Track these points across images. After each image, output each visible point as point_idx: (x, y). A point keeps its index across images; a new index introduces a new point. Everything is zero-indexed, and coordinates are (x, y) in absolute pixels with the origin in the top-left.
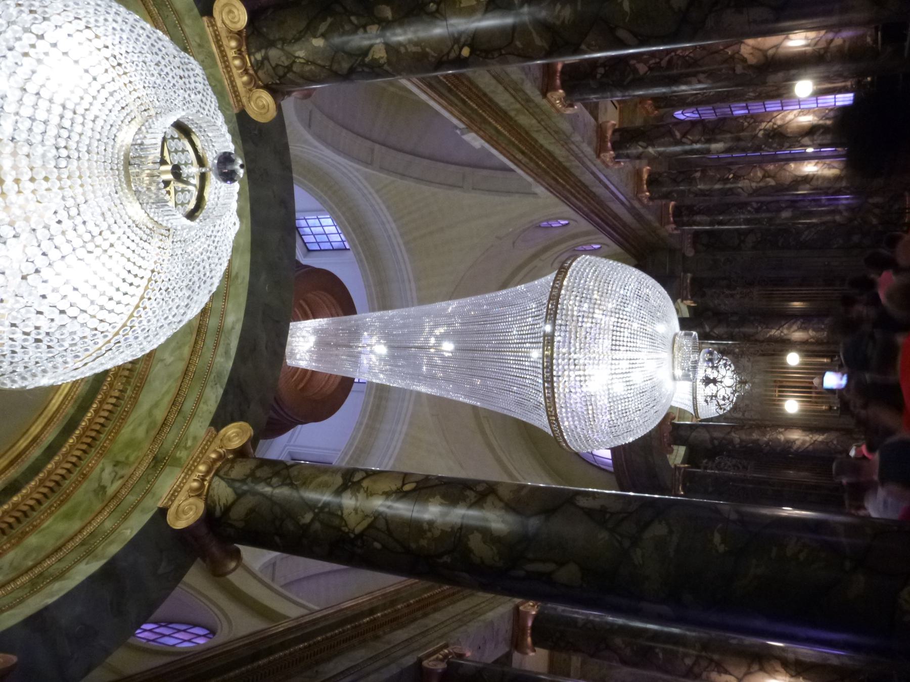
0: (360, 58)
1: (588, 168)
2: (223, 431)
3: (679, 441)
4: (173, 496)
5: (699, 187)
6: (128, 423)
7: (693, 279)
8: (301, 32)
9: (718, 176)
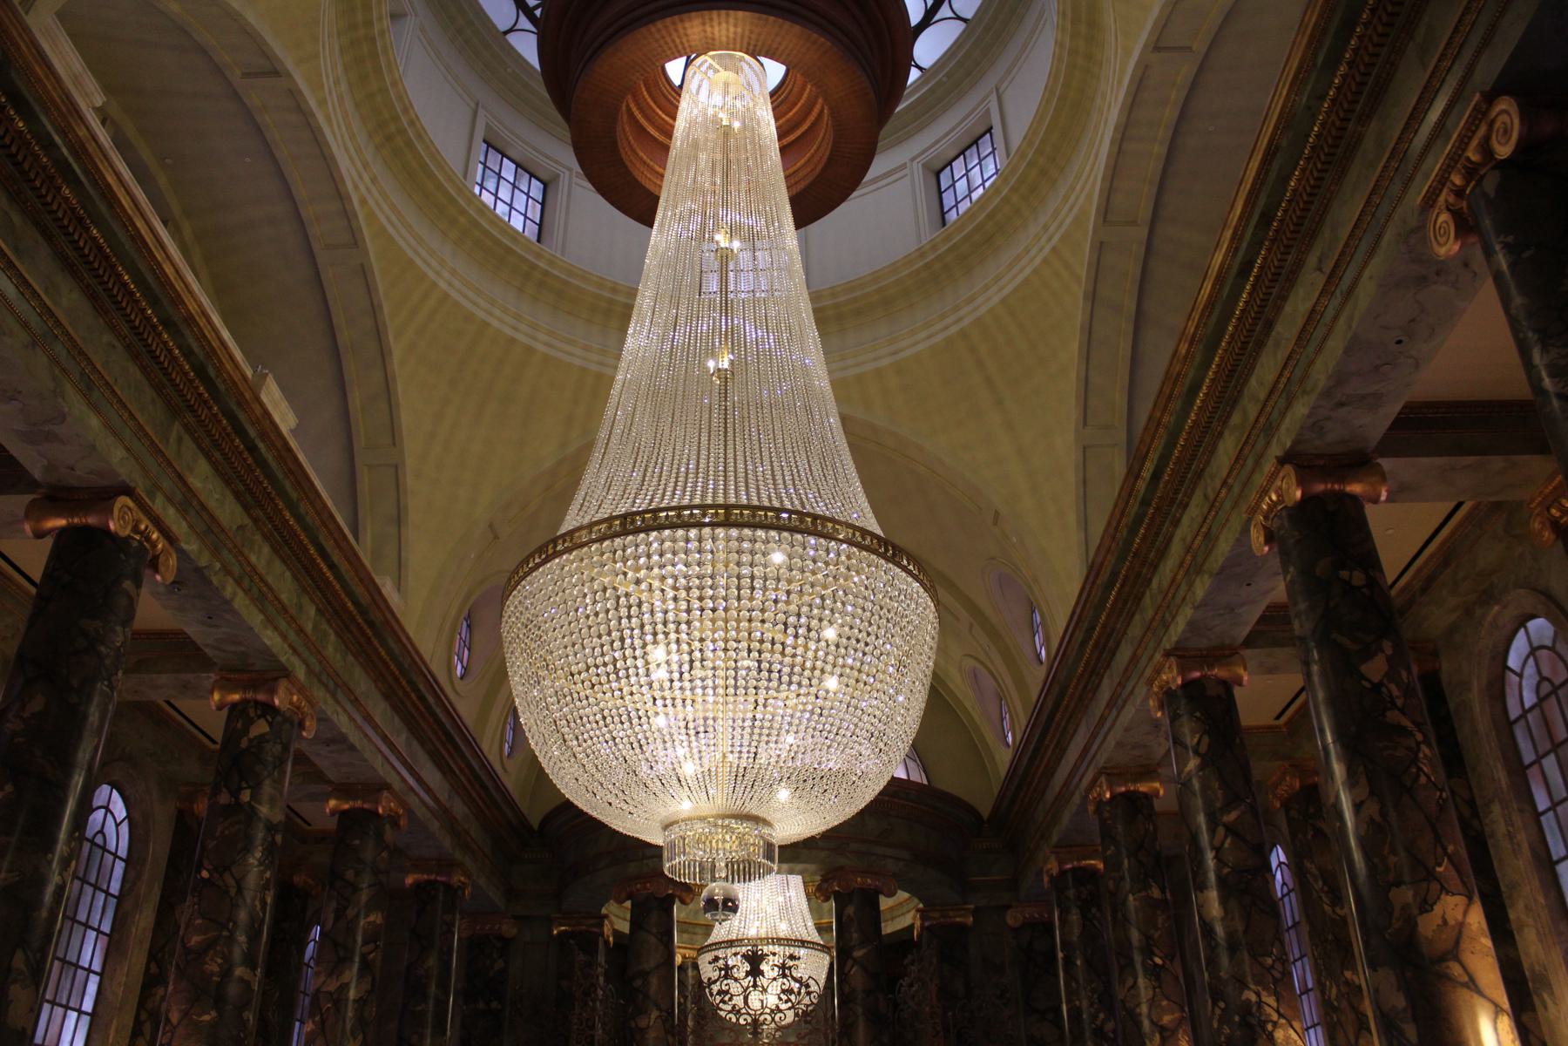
5: (1131, 898)
7: (962, 928)
9: (1156, 935)
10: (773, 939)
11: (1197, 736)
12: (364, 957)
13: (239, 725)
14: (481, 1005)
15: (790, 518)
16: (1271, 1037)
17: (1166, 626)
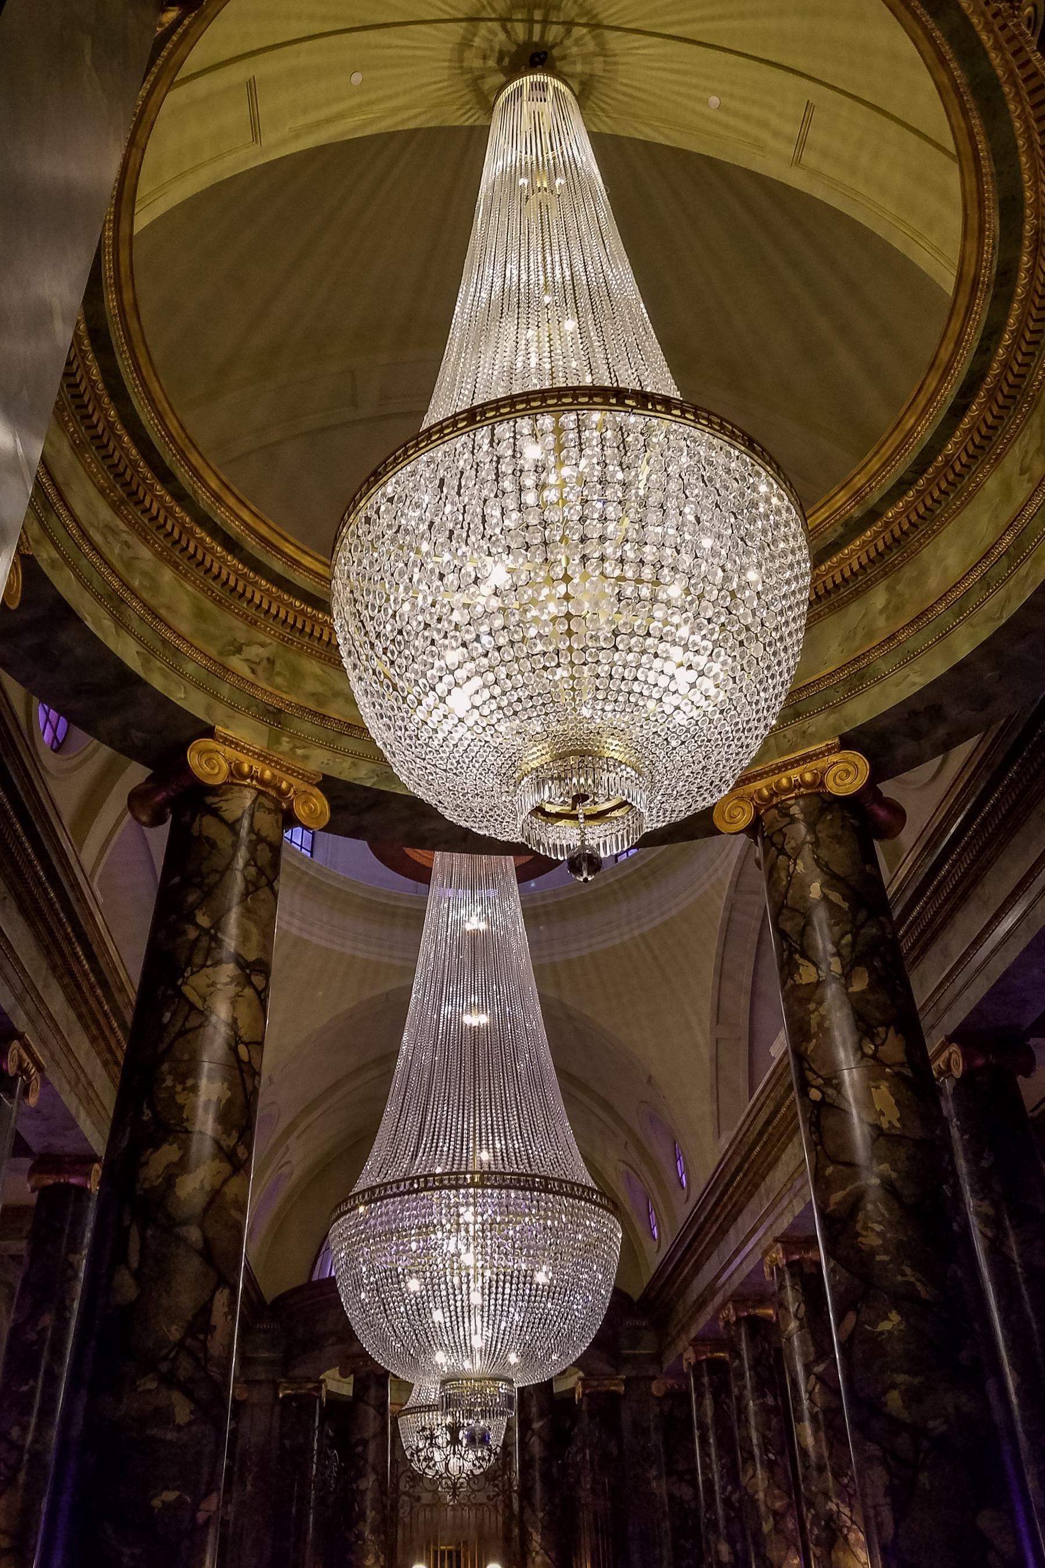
0: (798, 947)
1: (761, 1221)
2: (317, 791)
3: (361, 1386)
4: (227, 741)
5: (751, 1403)
6: (323, 667)
8: (827, 867)
16: (846, 1537)
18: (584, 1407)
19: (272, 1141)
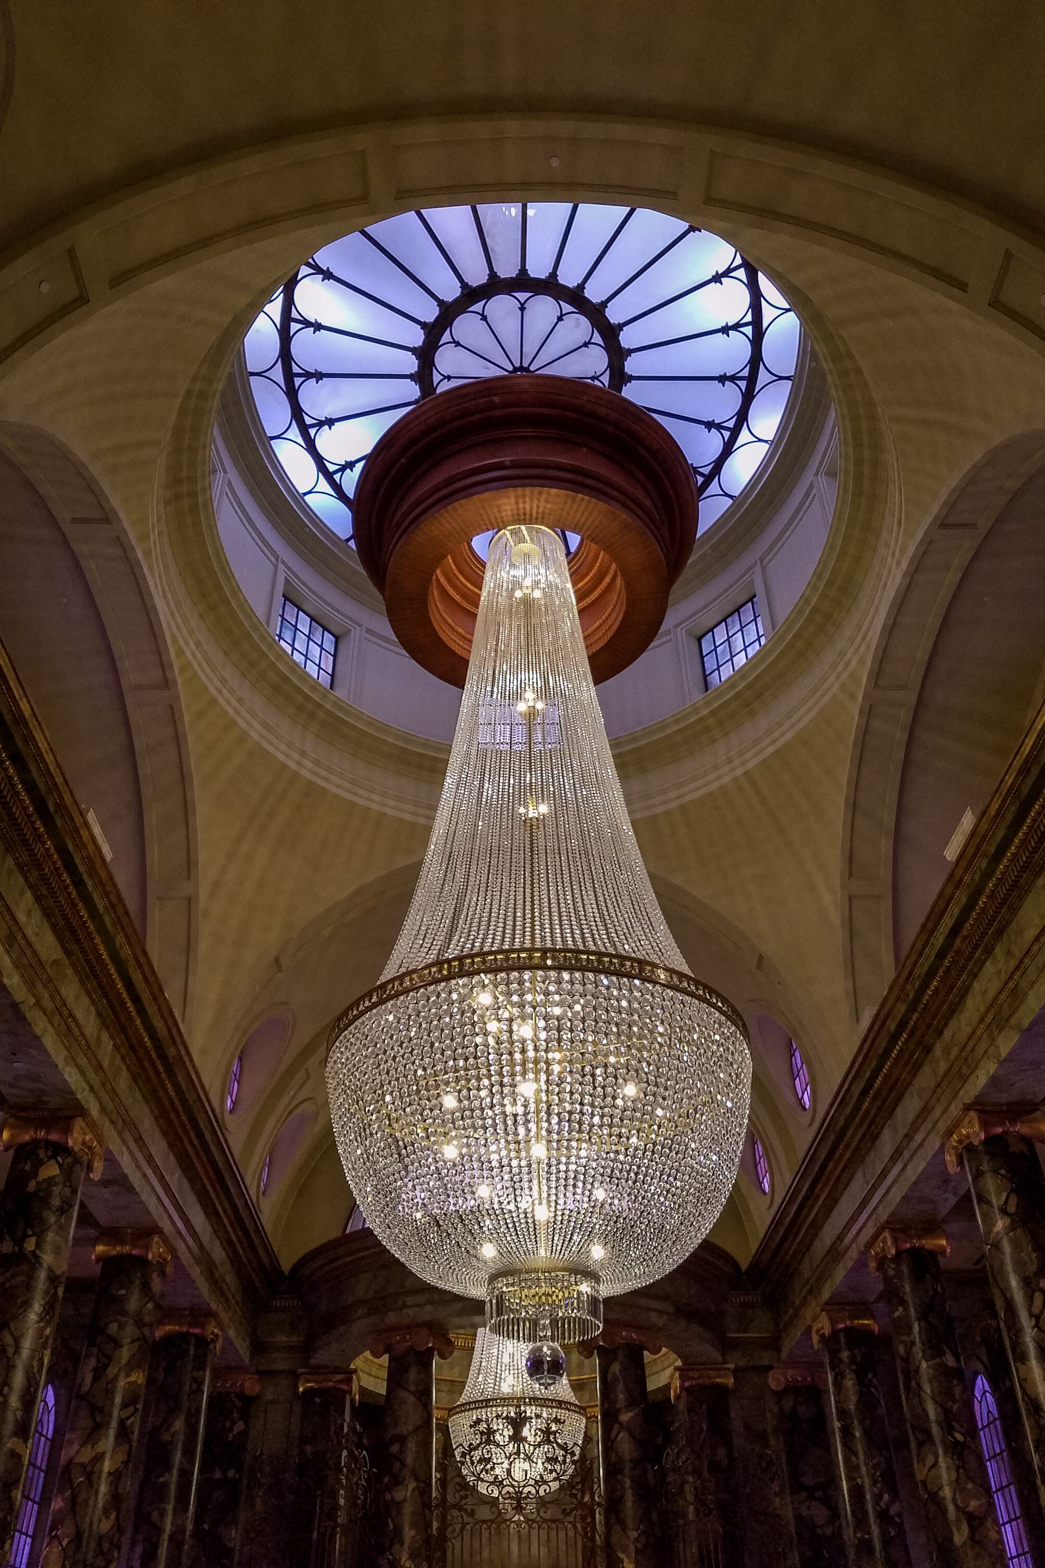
5: (924, 1365)
7: (723, 1389)
9: (955, 1407)
10: (530, 1399)
11: (1005, 1195)
12: (122, 1423)
13: (27, 1167)
14: (218, 1475)
15: (611, 962)
17: (964, 1079)
18: (682, 1406)
19: (287, 1061)
